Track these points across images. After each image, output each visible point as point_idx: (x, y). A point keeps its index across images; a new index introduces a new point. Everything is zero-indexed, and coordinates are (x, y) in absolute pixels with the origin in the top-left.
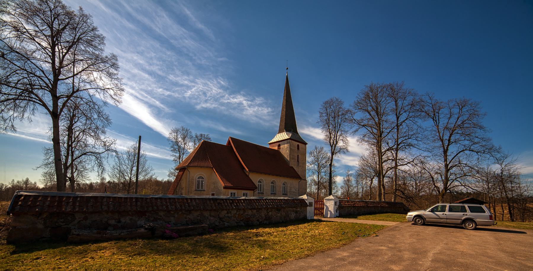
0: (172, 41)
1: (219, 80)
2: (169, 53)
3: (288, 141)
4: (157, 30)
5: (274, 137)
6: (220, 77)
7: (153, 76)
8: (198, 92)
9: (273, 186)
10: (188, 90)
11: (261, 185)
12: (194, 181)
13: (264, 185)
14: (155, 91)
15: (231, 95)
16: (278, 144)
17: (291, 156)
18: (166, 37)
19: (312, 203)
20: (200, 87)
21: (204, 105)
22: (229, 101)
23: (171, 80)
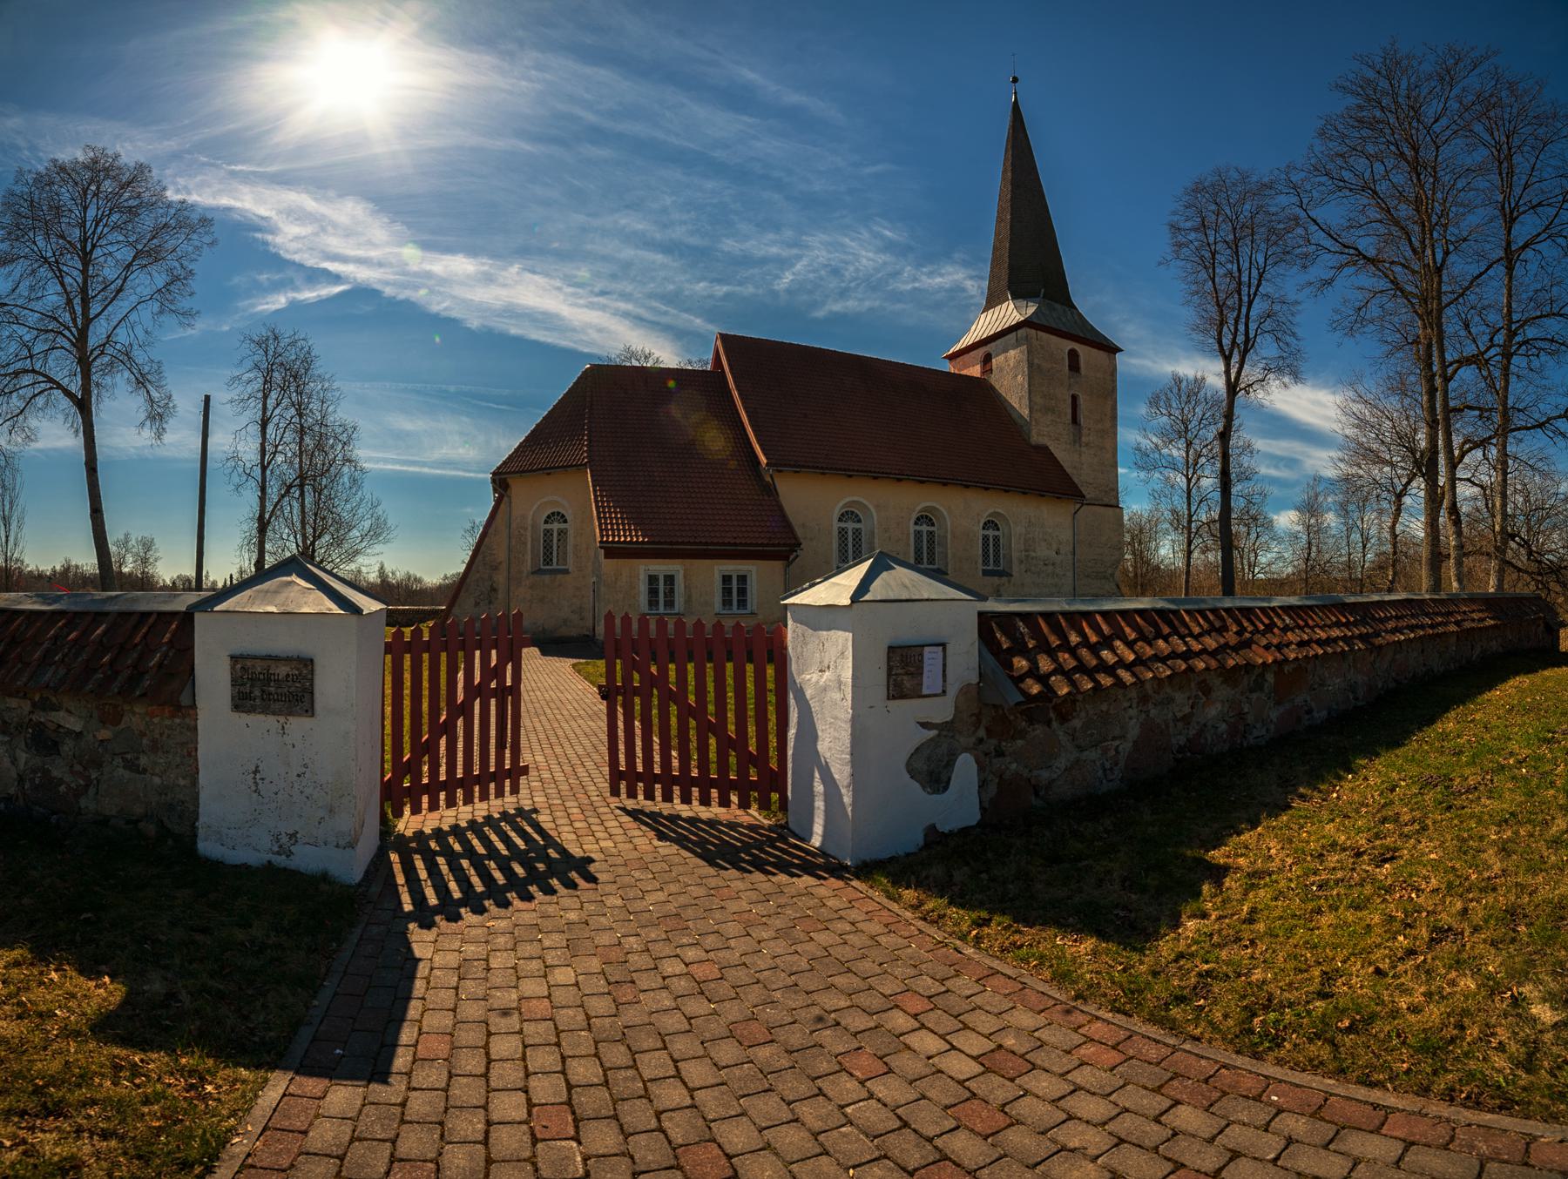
1: (876, 228)
2: (710, 185)
3: (1022, 332)
6: (878, 219)
8: (814, 271)
12: (529, 534)
13: (873, 533)
14: (687, 293)
15: (923, 266)
16: (981, 352)
17: (1038, 400)
19: (981, 614)
20: (818, 257)
21: (837, 307)
22: (917, 285)
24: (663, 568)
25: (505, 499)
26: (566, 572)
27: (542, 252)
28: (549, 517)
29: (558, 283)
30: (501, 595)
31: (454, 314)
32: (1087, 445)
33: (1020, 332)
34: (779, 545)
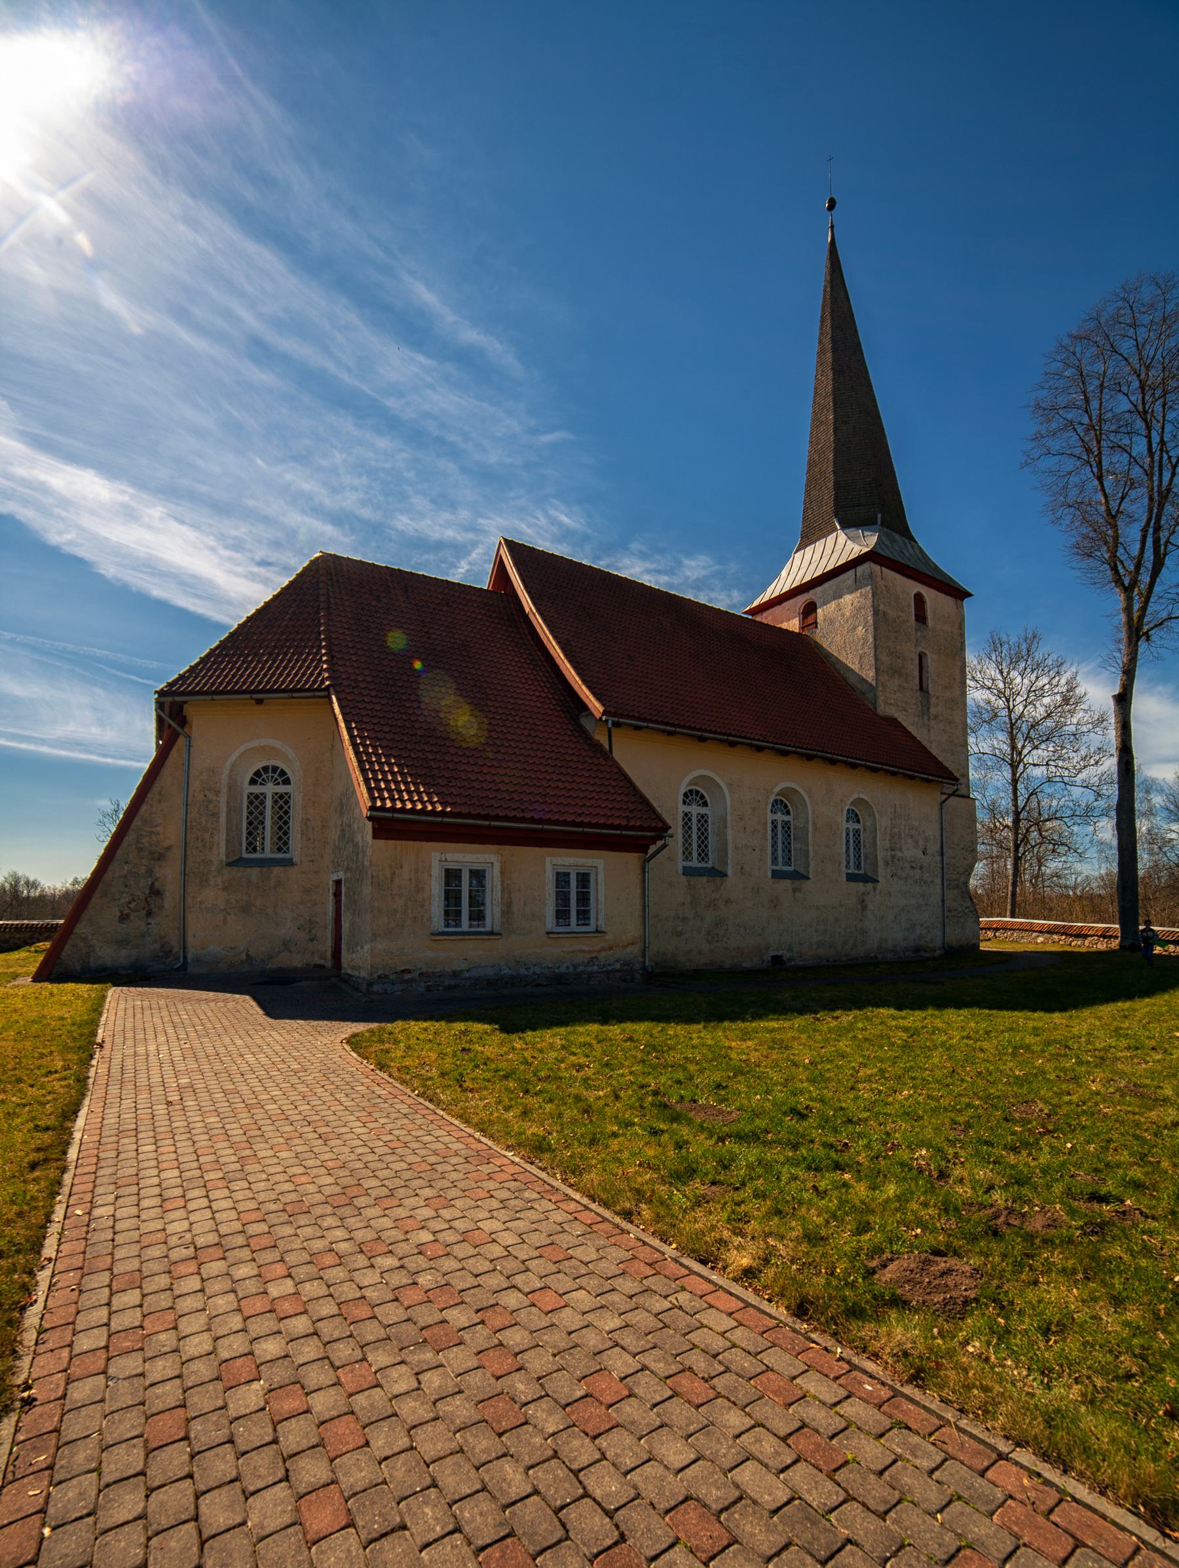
0: (391, 403)
1: (552, 512)
2: (383, 443)
4: (344, 376)
5: (778, 573)
7: (347, 527)
9: (786, 824)
10: (458, 558)
11: (703, 818)
12: (223, 799)
13: (724, 820)
17: (884, 658)
18: (370, 393)
23: (403, 531)
24: (470, 857)
25: (181, 741)
26: (290, 863)
27: (193, 498)
28: (258, 774)
29: (211, 541)
30: (170, 901)
31: (81, 552)
32: (936, 718)
33: (860, 569)
34: (641, 828)
